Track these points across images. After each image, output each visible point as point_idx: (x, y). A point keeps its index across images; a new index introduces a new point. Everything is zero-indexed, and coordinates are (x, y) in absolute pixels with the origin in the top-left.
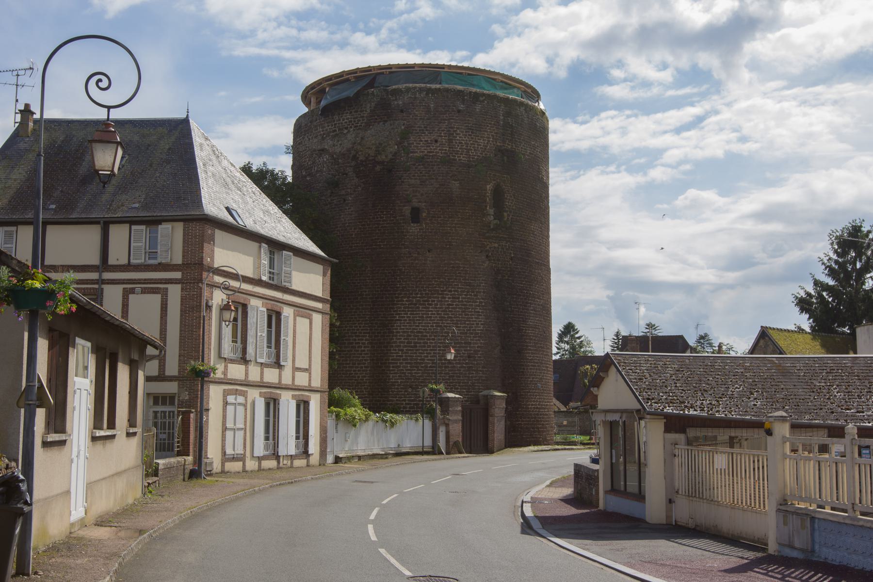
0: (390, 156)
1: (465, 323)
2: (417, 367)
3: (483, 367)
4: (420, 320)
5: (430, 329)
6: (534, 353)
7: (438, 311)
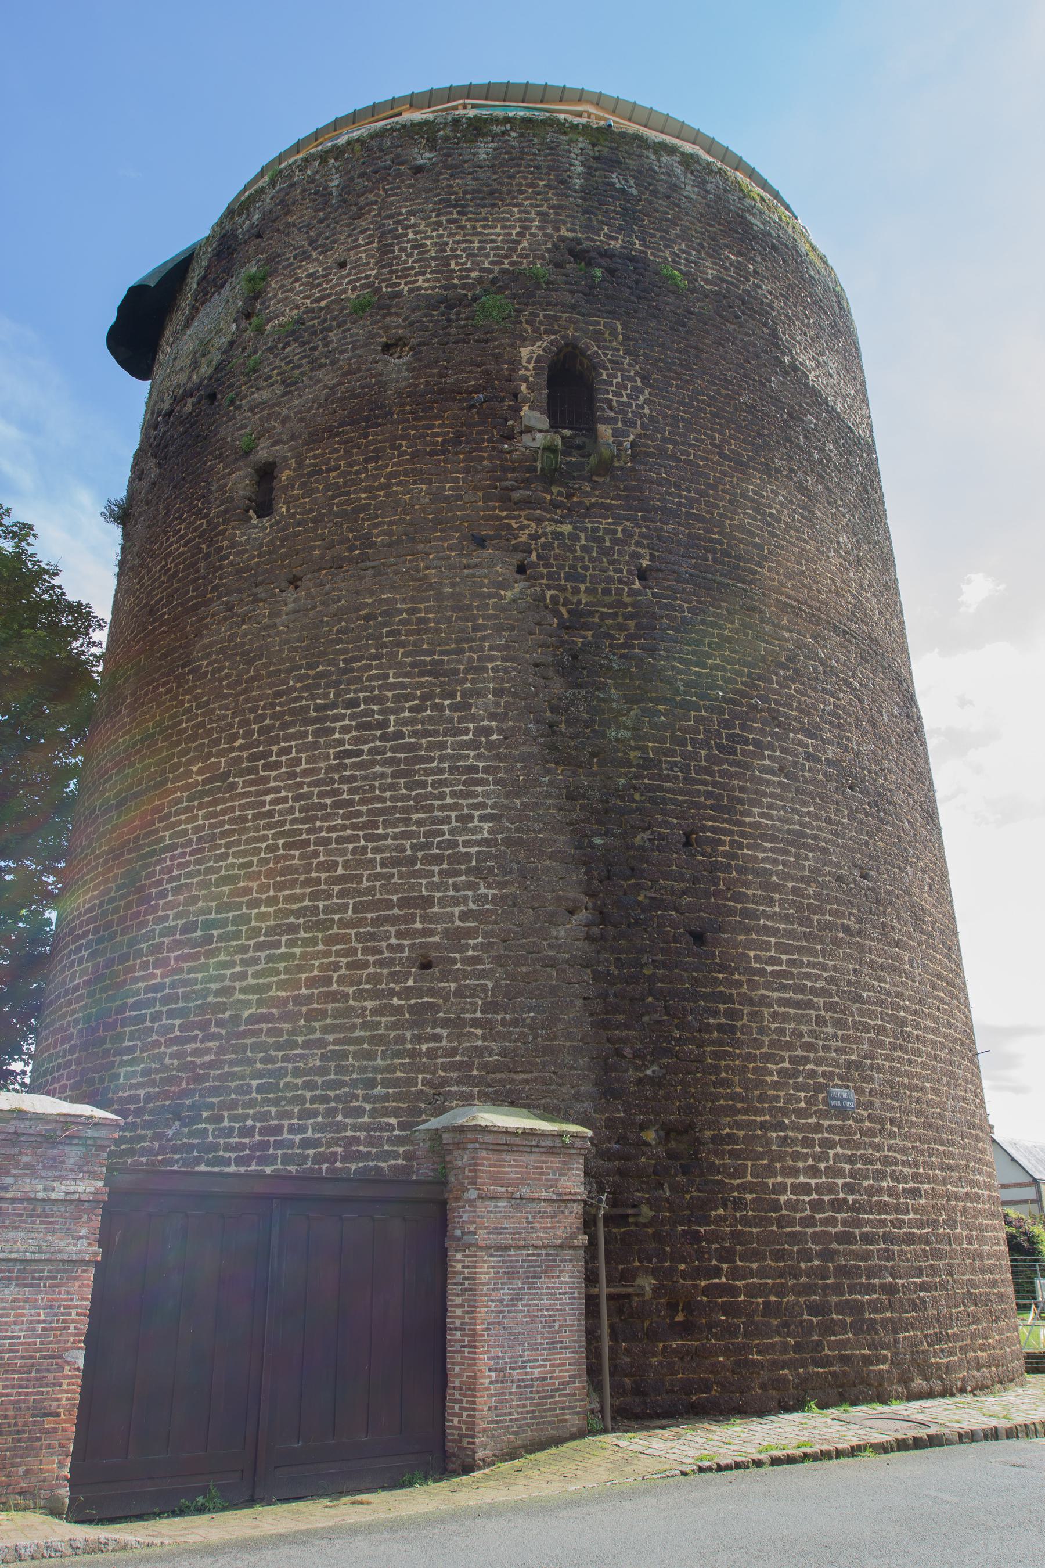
1: (407, 821)
2: (204, 1026)
3: (490, 1007)
4: (231, 832)
5: (263, 862)
6: (800, 950)
7: (300, 785)
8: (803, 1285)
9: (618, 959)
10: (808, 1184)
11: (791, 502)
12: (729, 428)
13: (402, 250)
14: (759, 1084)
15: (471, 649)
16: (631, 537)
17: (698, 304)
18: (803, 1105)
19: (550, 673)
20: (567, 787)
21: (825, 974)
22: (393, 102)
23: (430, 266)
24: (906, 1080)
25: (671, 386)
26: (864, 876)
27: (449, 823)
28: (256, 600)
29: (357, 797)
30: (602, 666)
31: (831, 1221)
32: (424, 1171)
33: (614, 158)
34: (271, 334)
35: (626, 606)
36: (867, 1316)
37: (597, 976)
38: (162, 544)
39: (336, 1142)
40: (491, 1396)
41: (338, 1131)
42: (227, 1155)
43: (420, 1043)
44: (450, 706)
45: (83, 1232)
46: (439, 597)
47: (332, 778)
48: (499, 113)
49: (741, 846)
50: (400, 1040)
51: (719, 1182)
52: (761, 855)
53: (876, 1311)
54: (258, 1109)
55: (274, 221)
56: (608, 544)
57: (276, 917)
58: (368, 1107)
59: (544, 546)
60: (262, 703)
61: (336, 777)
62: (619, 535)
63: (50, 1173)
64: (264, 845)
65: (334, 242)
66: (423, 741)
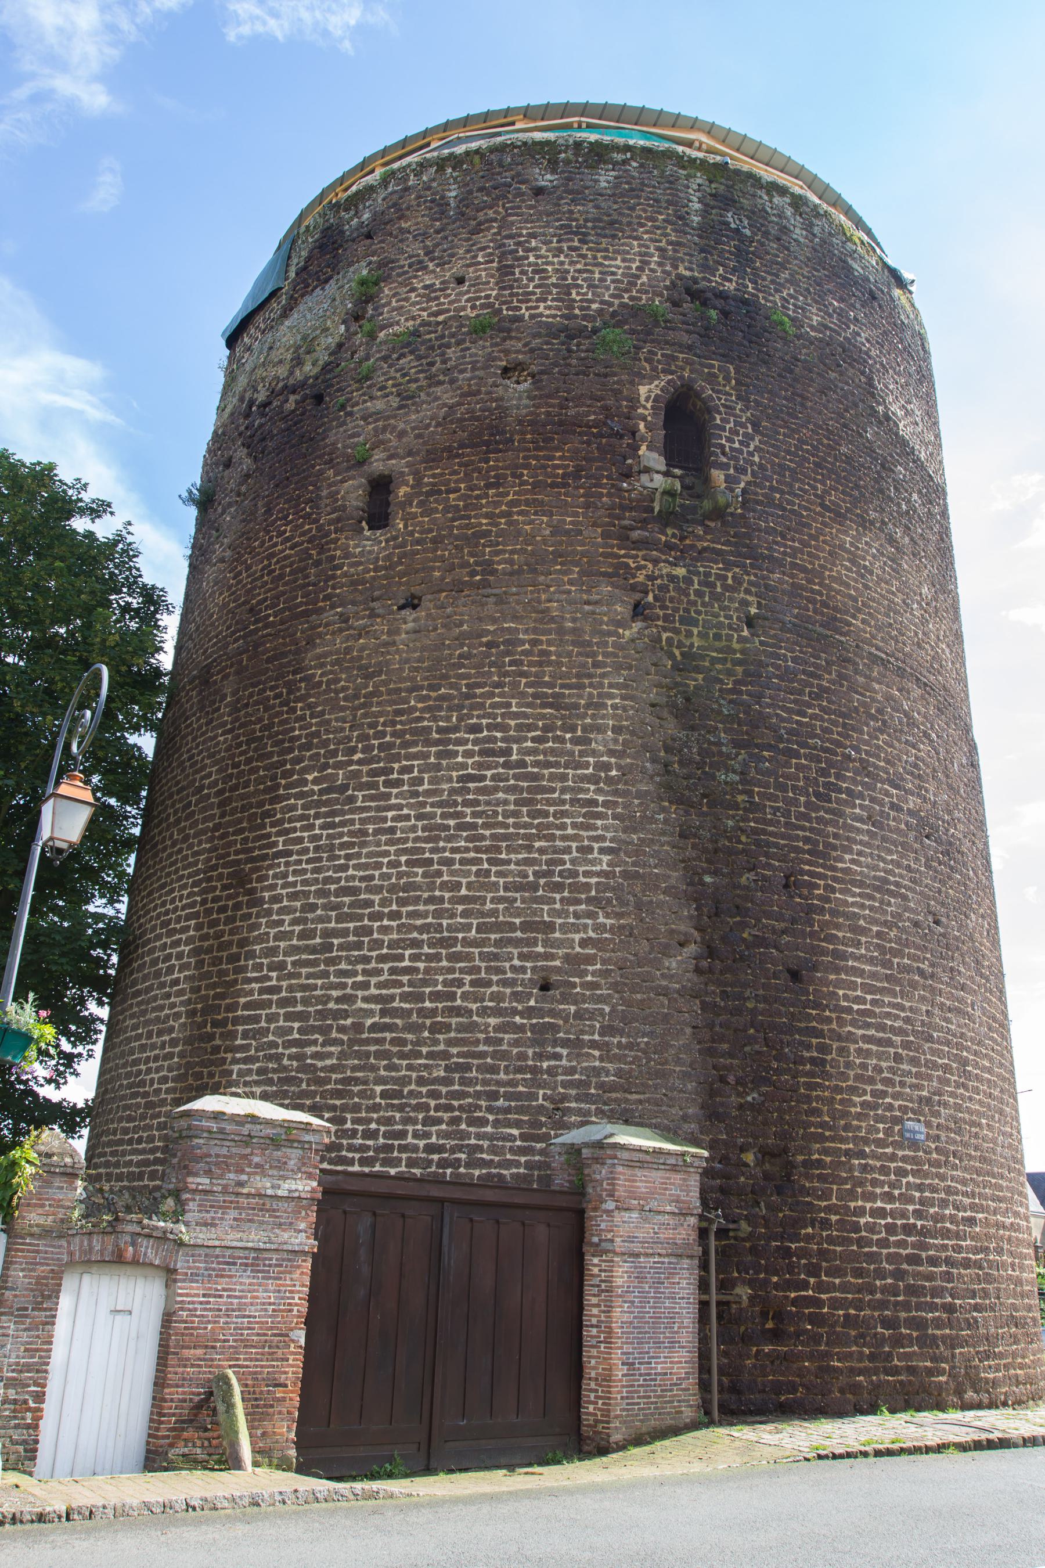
0: (324, 358)
1: (529, 848)
2: (325, 1030)
4: (352, 845)
5: (384, 877)
6: (882, 991)
7: (423, 805)
8: (878, 1300)
9: (723, 992)
10: (884, 1209)
11: (882, 554)
12: (830, 479)
13: (522, 273)
14: (845, 1114)
15: (591, 685)
16: (740, 584)
17: (804, 351)
18: (881, 1135)
19: (665, 714)
20: (681, 826)
21: (903, 1015)
22: (508, 112)
23: (551, 293)
24: (967, 1116)
25: (779, 433)
26: (937, 922)
27: (570, 853)
28: (373, 615)
29: (480, 821)
30: (712, 710)
31: (901, 1244)
32: (560, 1181)
33: (729, 195)
34: (385, 342)
35: (735, 652)
36: (930, 1331)
37: (704, 1006)
38: (263, 543)
39: (460, 1149)
40: (623, 1386)
41: (462, 1139)
42: (350, 1155)
43: (541, 1061)
44: (571, 740)
45: (302, 1226)
46: (561, 631)
47: (455, 801)
48: (620, 141)
49: (833, 890)
50: (522, 1056)
51: (810, 1203)
52: (850, 900)
53: (938, 1328)
54: (381, 1113)
55: (386, 224)
56: (719, 590)
57: (399, 932)
58: (491, 1118)
59: (661, 588)
60: (382, 720)
61: (460, 800)
62: (730, 581)
63: (275, 1172)
64: (386, 860)
65: (453, 255)
66: (546, 772)
